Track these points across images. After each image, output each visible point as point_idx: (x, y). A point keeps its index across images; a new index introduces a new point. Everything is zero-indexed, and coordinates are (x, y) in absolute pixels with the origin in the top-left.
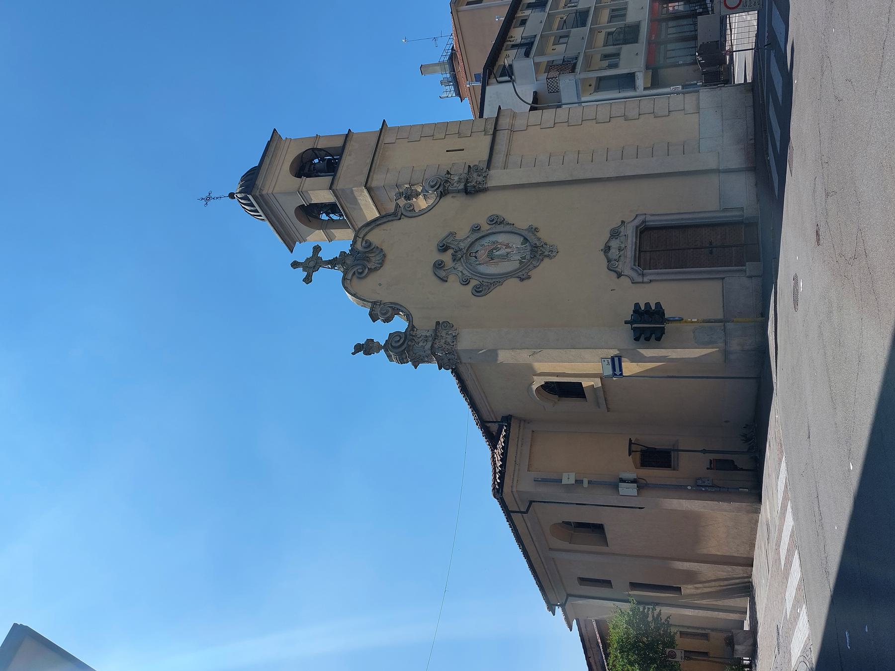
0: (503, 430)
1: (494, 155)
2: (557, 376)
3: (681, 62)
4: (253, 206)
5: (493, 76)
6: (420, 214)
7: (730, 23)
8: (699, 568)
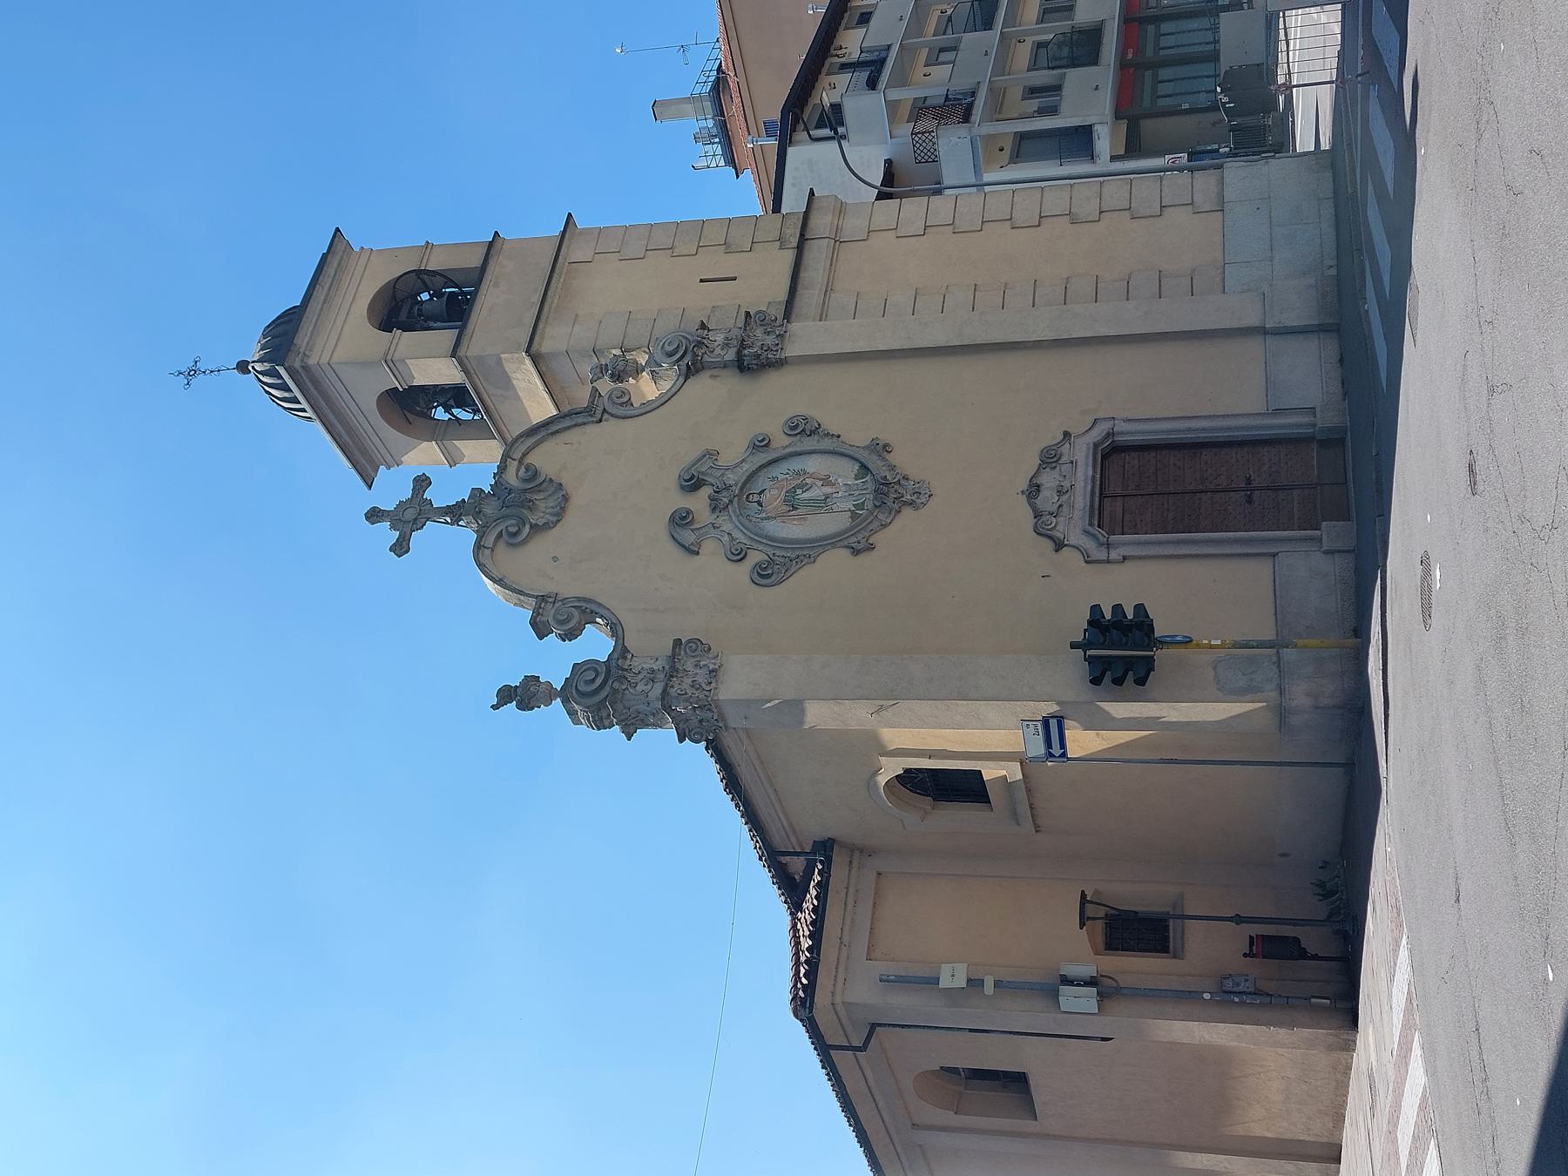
0: (817, 870)
1: (800, 291)
5: (802, 126)
6: (642, 411)
7: (1285, 29)
8: (1227, 1165)
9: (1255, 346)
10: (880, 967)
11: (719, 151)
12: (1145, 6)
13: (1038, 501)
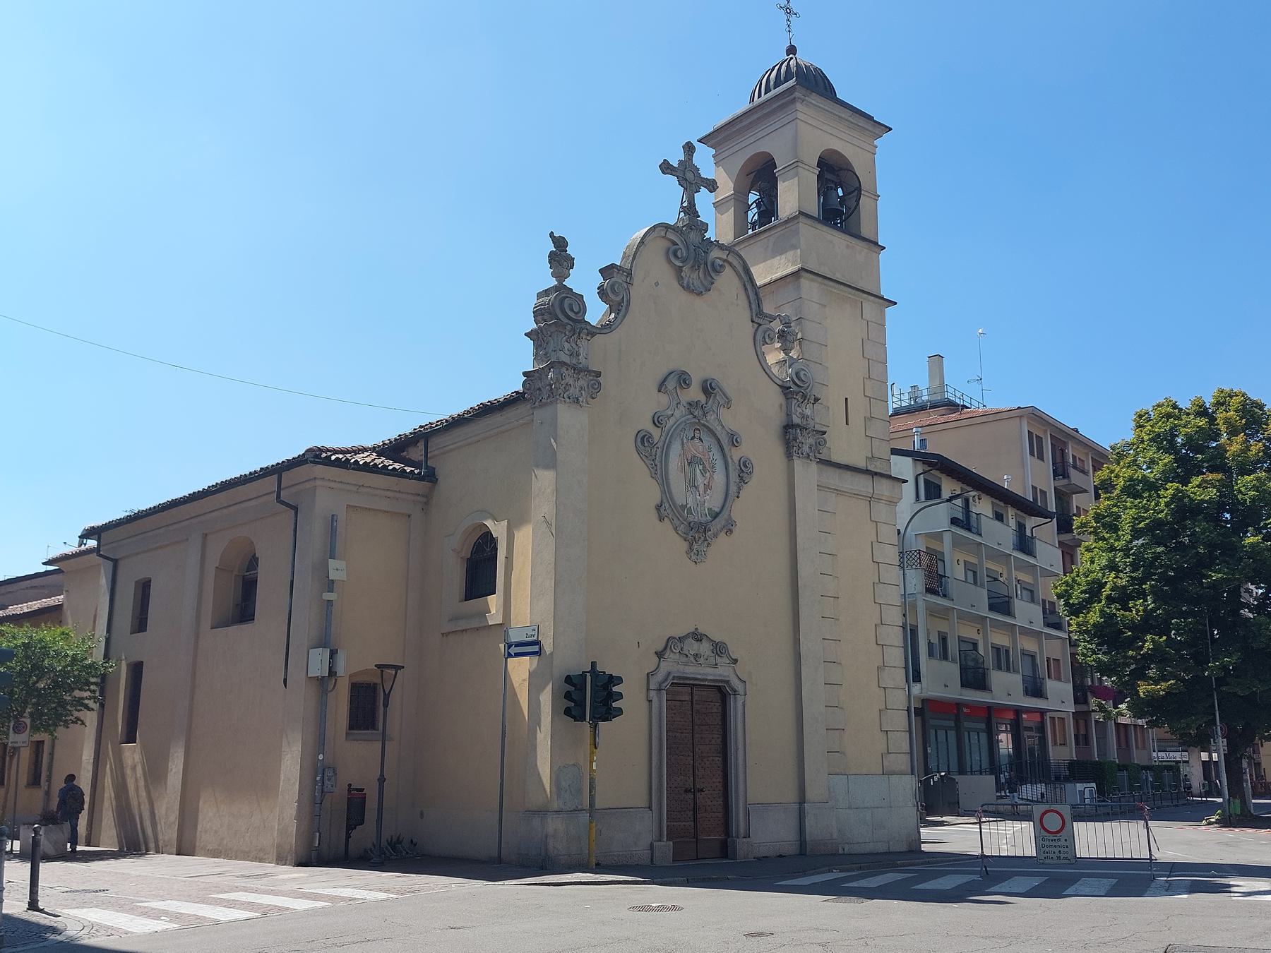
0: (413, 469)
1: (838, 471)
3: (929, 751)
6: (759, 353)
7: (989, 821)
8: (174, 770)
9: (791, 796)
11: (904, 404)
12: (999, 721)
13: (690, 639)
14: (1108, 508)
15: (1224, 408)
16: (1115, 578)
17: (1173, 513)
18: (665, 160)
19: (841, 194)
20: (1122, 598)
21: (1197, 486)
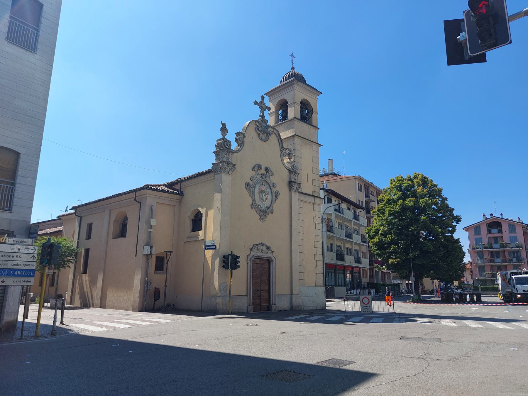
1: (304, 195)
2: (205, 219)
4: (288, 79)
5: (328, 194)
9: (288, 292)
10: (155, 205)
13: (260, 245)
14: (382, 207)
15: (416, 178)
16: (383, 228)
17: (401, 209)
18: (255, 101)
19: (307, 112)
20: (385, 234)
21: (408, 202)
